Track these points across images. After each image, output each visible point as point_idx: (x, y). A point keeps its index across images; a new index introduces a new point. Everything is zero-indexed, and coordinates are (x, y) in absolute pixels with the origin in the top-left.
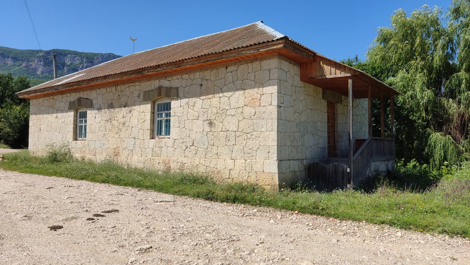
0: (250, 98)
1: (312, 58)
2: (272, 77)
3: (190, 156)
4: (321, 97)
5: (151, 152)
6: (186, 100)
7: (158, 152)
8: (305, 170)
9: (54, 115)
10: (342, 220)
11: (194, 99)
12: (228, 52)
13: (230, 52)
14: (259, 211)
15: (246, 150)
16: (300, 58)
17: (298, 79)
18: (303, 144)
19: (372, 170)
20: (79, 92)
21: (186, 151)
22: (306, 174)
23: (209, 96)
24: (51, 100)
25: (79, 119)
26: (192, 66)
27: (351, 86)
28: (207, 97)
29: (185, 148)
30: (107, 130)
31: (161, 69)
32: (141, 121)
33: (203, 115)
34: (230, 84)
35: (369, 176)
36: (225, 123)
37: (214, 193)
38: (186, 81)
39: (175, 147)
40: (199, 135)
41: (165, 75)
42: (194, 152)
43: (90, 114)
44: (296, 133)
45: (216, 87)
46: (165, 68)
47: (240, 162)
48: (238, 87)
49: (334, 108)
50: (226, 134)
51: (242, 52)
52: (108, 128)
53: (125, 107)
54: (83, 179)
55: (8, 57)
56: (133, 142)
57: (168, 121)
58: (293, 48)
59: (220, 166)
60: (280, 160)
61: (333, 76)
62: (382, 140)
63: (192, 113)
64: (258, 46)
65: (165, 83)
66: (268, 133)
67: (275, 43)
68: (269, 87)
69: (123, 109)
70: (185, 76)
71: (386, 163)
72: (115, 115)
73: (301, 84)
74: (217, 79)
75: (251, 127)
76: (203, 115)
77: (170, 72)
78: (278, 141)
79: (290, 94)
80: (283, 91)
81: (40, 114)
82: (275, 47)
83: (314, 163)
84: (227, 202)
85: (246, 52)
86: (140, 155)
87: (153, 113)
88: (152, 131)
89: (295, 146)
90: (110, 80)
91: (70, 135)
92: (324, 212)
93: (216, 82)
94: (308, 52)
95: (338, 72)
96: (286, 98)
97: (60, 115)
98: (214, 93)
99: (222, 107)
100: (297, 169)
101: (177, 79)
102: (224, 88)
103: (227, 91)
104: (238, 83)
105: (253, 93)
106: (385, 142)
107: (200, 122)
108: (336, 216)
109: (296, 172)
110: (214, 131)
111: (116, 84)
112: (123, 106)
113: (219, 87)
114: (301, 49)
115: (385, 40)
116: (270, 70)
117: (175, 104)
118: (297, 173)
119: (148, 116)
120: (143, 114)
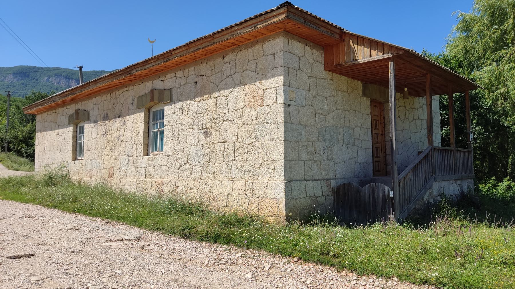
0: (251, 96)
1: (337, 36)
2: (277, 65)
3: (184, 176)
4: (361, 94)
5: (144, 173)
6: (180, 104)
7: (151, 172)
8: (333, 195)
9: (56, 131)
10: (361, 274)
11: (188, 102)
12: (220, 35)
13: (222, 34)
14: (244, 256)
15: (247, 166)
16: (327, 40)
17: (319, 69)
18: (330, 158)
19: (435, 193)
20: (77, 103)
21: (180, 171)
22: (334, 200)
23: (205, 96)
24: (54, 114)
25: (78, 135)
26: (182, 58)
27: (393, 72)
28: (202, 98)
29: (178, 167)
30: (103, 147)
31: (150, 65)
32: (134, 134)
33: (198, 122)
34: (228, 79)
35: (429, 203)
36: (223, 132)
37: (193, 227)
38: (180, 79)
39: (169, 165)
40: (194, 149)
41: (158, 73)
42: (188, 172)
43: (88, 127)
44: (318, 143)
45: (212, 85)
46: (153, 64)
47: (239, 183)
48: (237, 82)
49: (384, 110)
50: (223, 147)
51: (236, 32)
52: (103, 144)
53: (119, 117)
54: (55, 207)
55: (72, 79)
56: (127, 161)
57: (162, 132)
58: (302, 20)
59: (216, 191)
60: (289, 182)
61: (367, 59)
62: (452, 150)
63: (187, 120)
64: (254, 21)
65: (158, 84)
66: (273, 142)
67: (274, 13)
68: (274, 79)
69: (118, 120)
70: (179, 73)
71: (459, 182)
72: (110, 128)
73: (325, 74)
74: (213, 73)
75: (253, 136)
76: (198, 122)
77: (163, 70)
78: (285, 153)
79: (307, 88)
80: (294, 84)
81: (44, 131)
82: (275, 20)
83: (344, 184)
84: (207, 242)
85: (241, 31)
86: (133, 177)
87: (147, 123)
88: (147, 146)
89: (316, 161)
90: (101, 85)
91: (70, 154)
92: (336, 261)
93: (212, 77)
94: (329, 27)
95: (374, 53)
96: (299, 94)
97: (61, 131)
98: (209, 93)
99: (220, 109)
100: (319, 193)
101: (171, 78)
102: (221, 85)
103: (224, 89)
104: (237, 76)
105: (254, 87)
106: (458, 154)
107: (195, 132)
108: (353, 268)
109: (317, 197)
110: (210, 143)
111: (109, 90)
112: (117, 116)
113: (215, 84)
114: (317, 21)
115: (467, 27)
116: (274, 55)
117: (168, 110)
118: (319, 199)
119: (141, 127)
120: (136, 125)
